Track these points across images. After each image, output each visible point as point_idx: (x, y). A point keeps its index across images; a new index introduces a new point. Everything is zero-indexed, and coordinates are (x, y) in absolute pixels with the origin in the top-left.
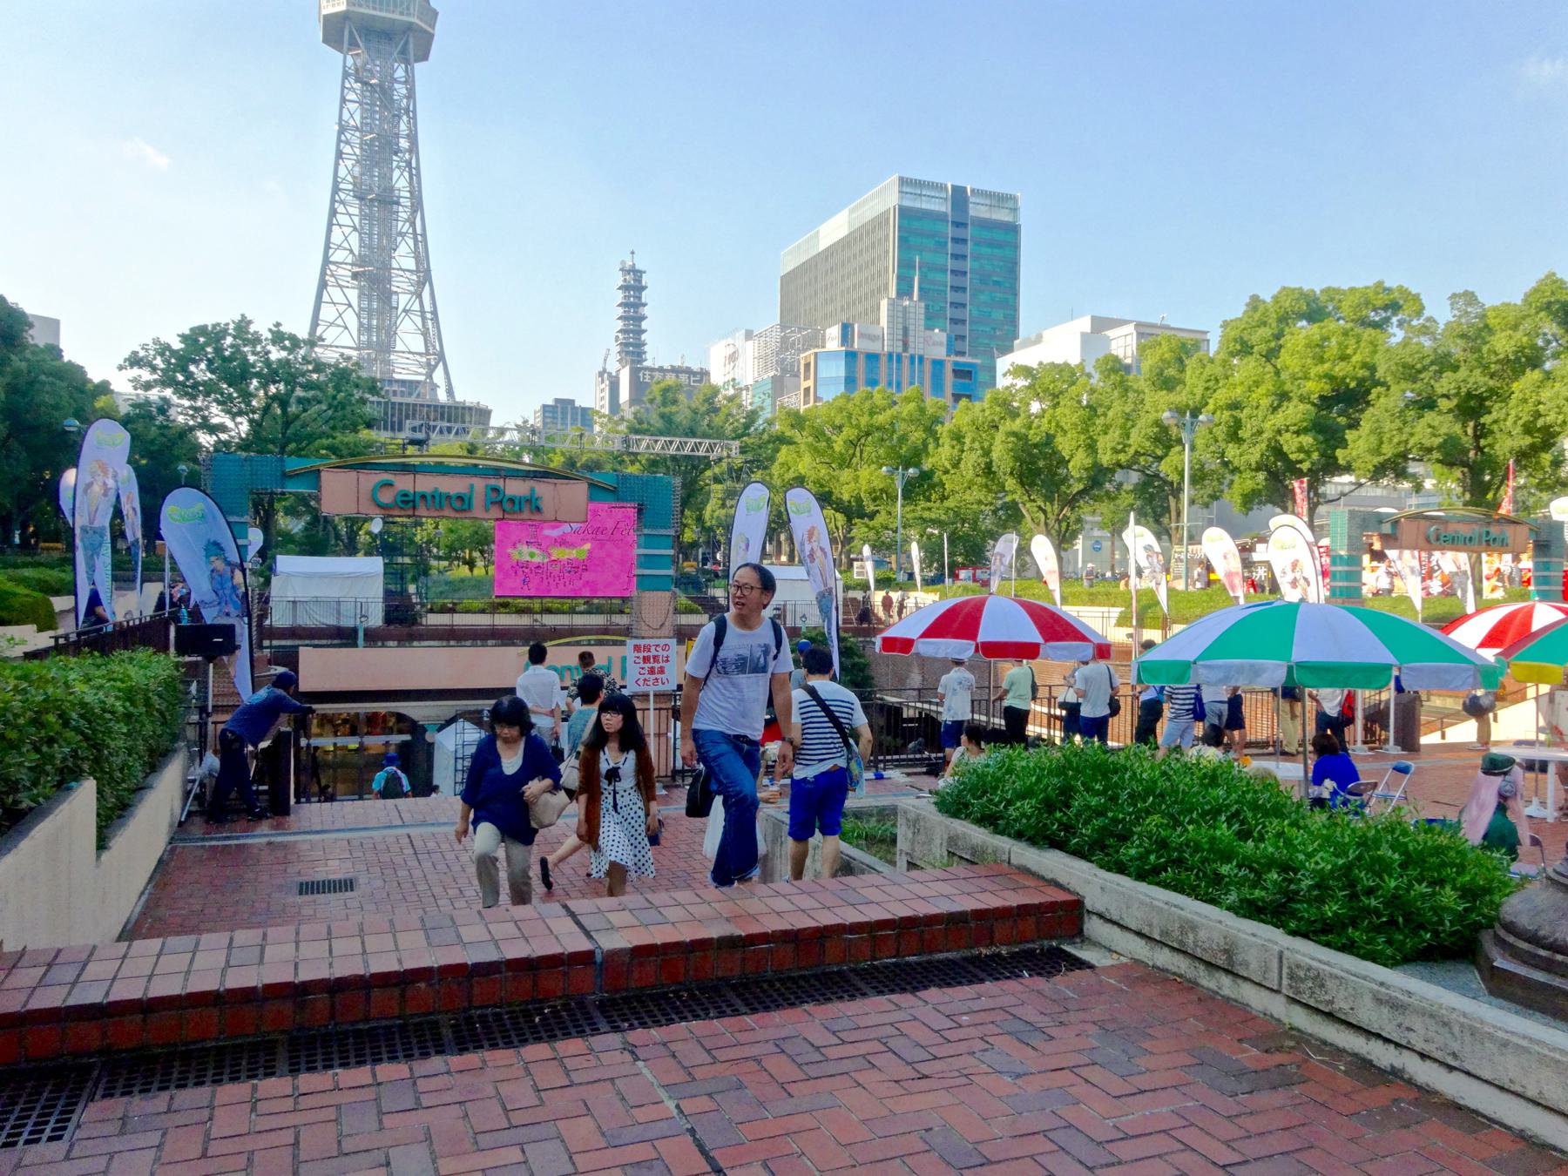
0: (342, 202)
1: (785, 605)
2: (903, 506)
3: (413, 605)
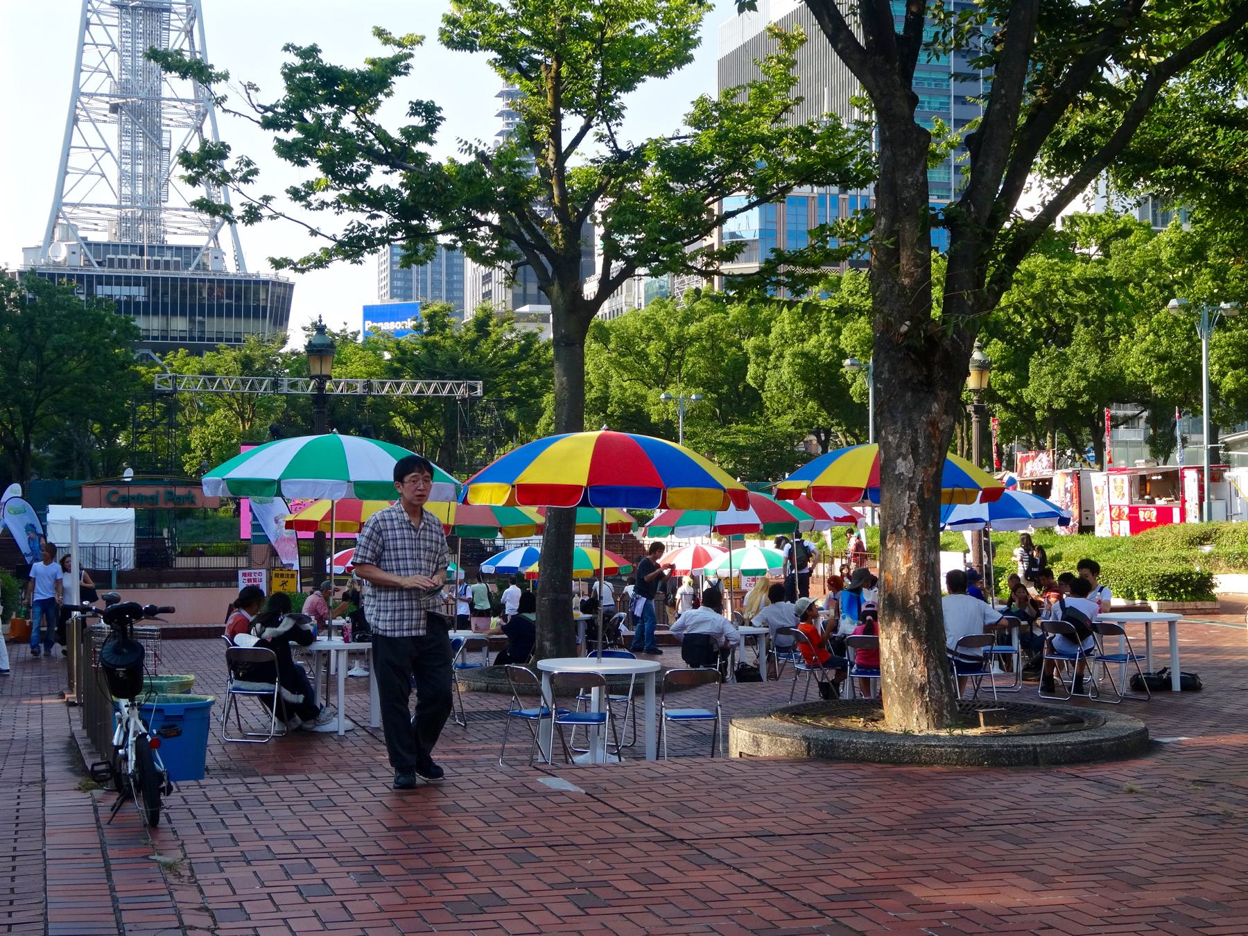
0: (97, 12)
3: (165, 549)
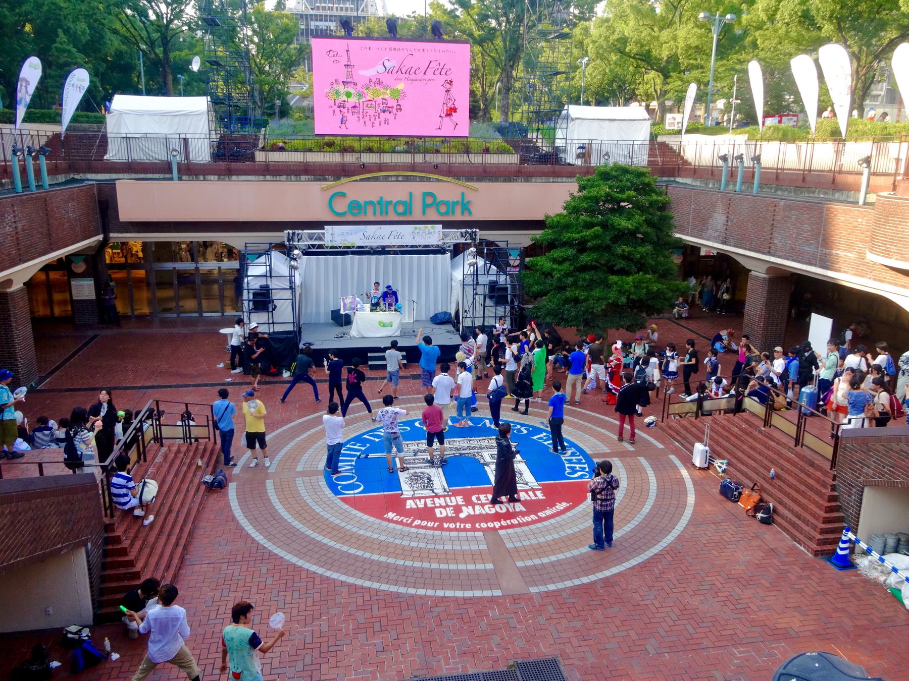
1: (590, 144)
2: (716, 60)
